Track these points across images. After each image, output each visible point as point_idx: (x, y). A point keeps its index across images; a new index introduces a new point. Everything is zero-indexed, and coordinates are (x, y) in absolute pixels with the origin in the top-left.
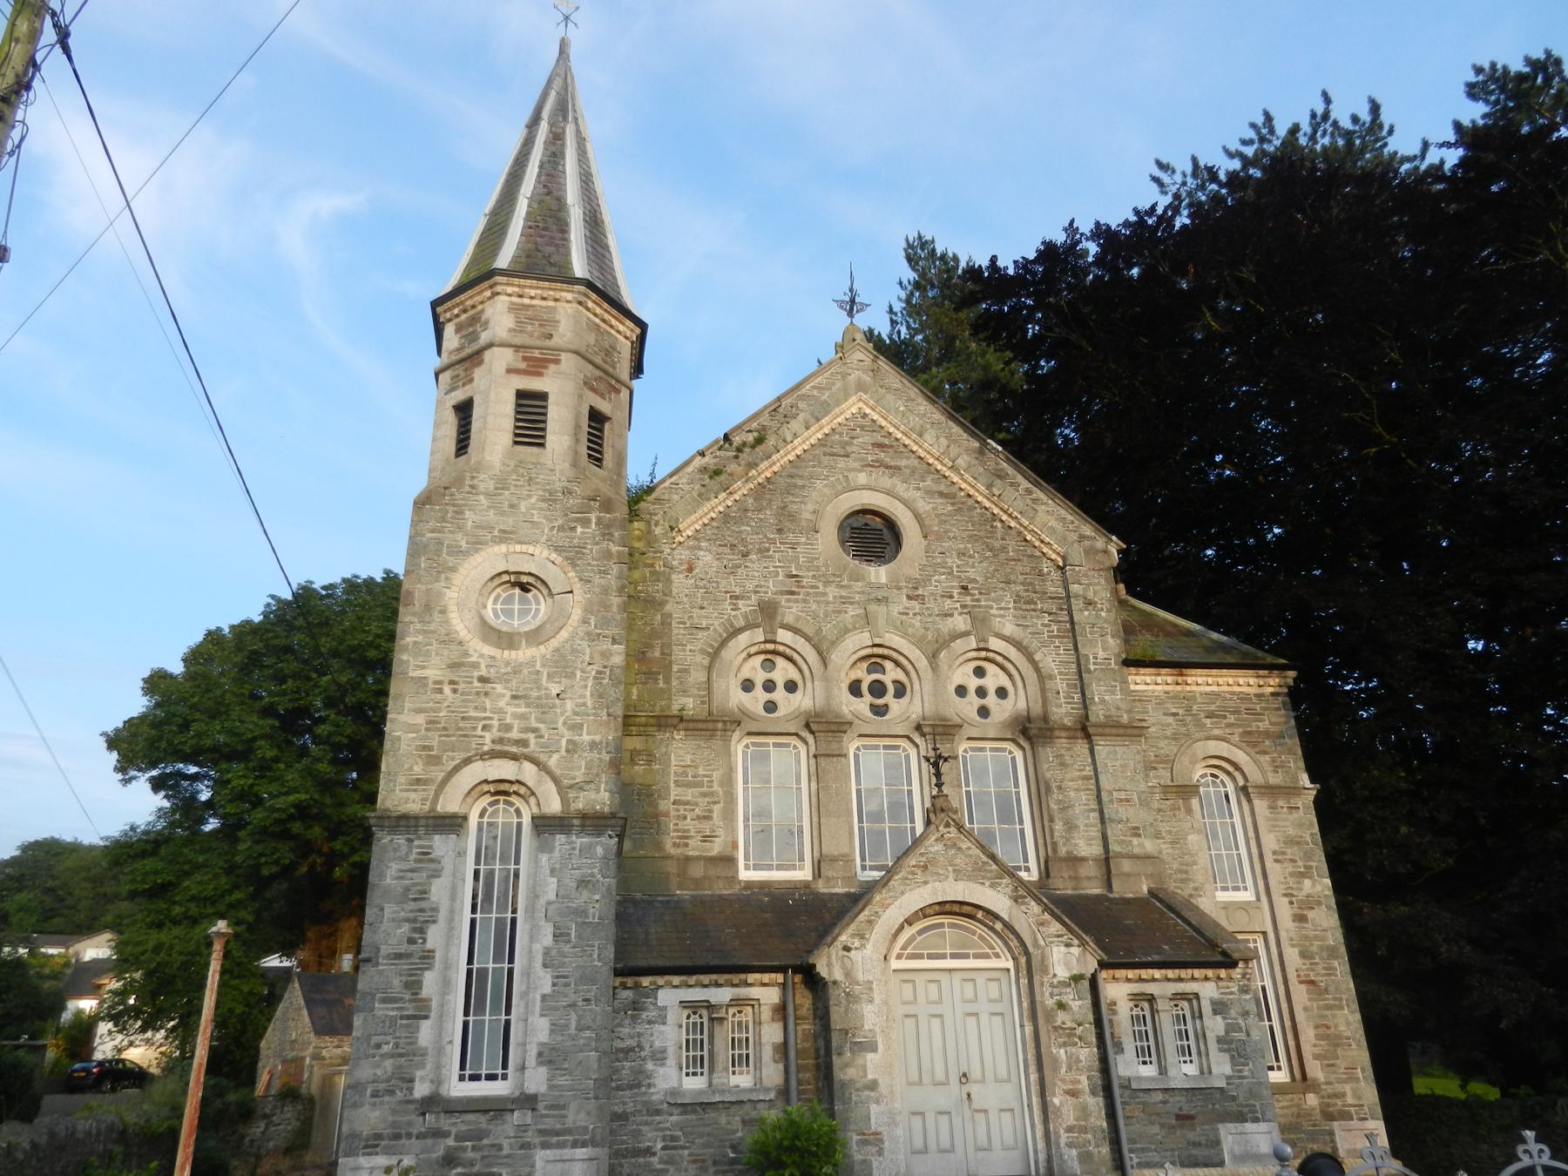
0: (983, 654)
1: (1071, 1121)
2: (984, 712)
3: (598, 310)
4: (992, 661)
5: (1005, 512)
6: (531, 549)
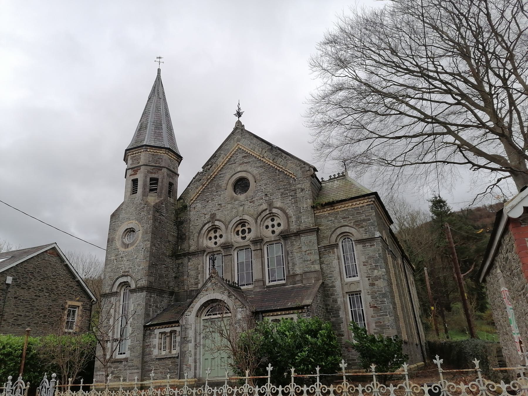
0: (272, 214)
2: (273, 232)
3: (152, 151)
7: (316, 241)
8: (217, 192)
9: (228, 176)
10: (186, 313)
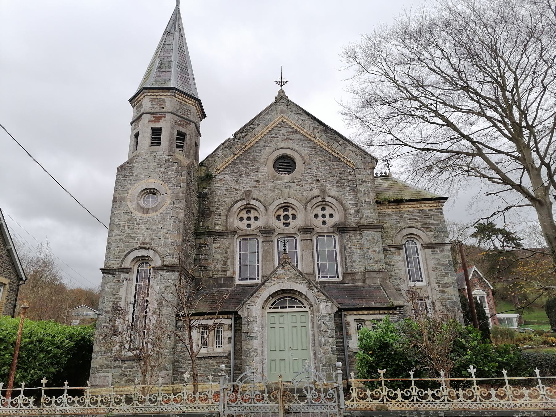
0: (324, 203)
2: (324, 223)
3: (180, 97)
5: (333, 151)
7: (380, 239)
8: (253, 166)
9: (268, 150)
10: (248, 302)
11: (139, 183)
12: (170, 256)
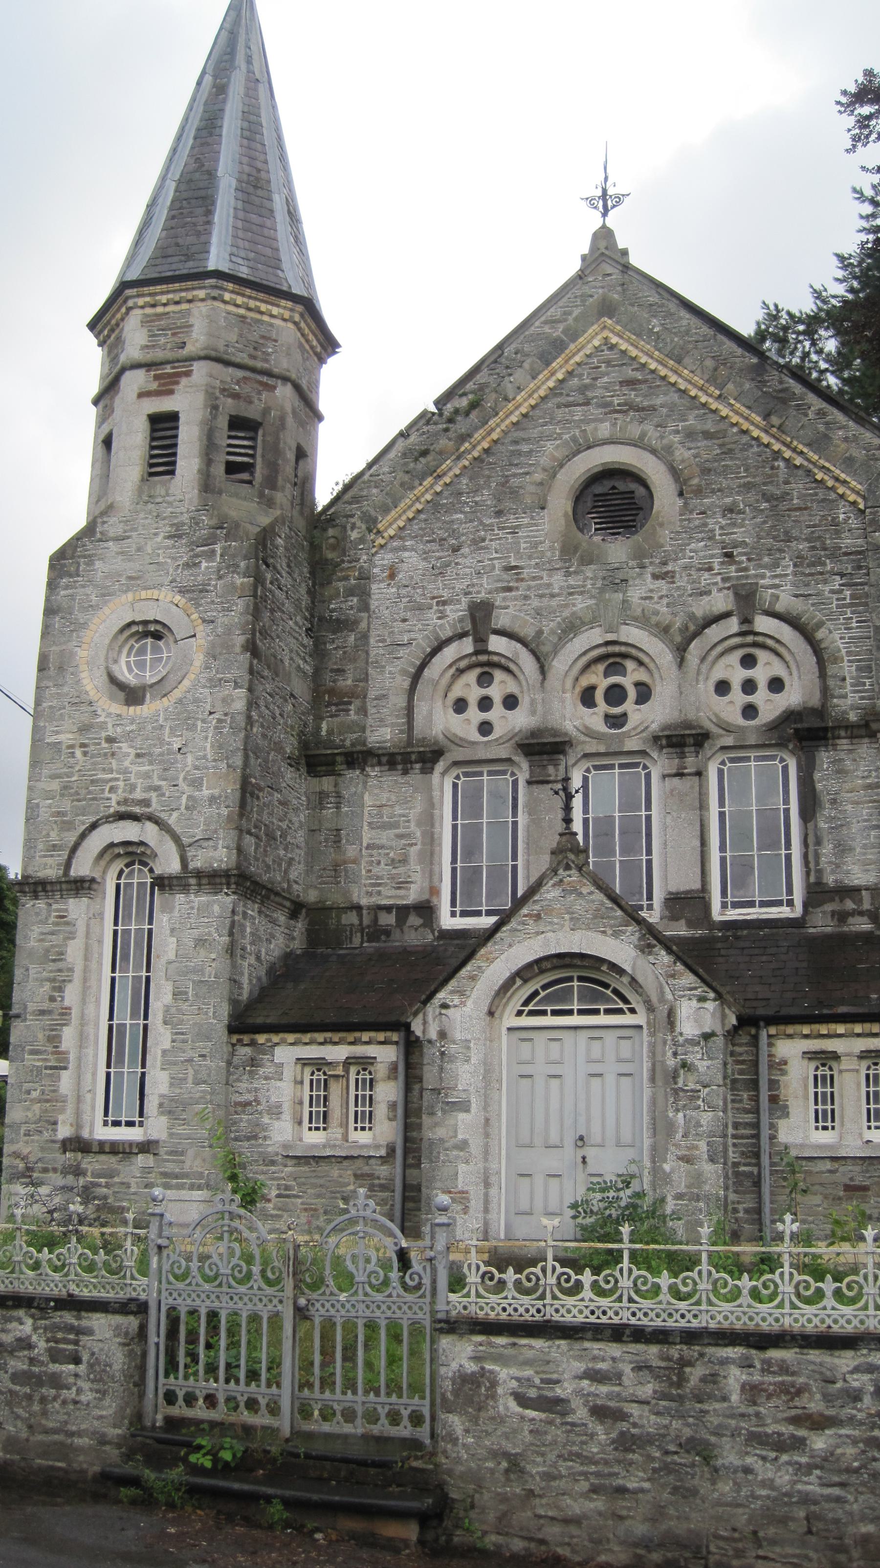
0: (750, 639)
1: (682, 1189)
3: (240, 300)
4: (763, 646)
5: (788, 446)
6: (155, 594)
8: (499, 513)
11: (111, 605)
12: (205, 844)
